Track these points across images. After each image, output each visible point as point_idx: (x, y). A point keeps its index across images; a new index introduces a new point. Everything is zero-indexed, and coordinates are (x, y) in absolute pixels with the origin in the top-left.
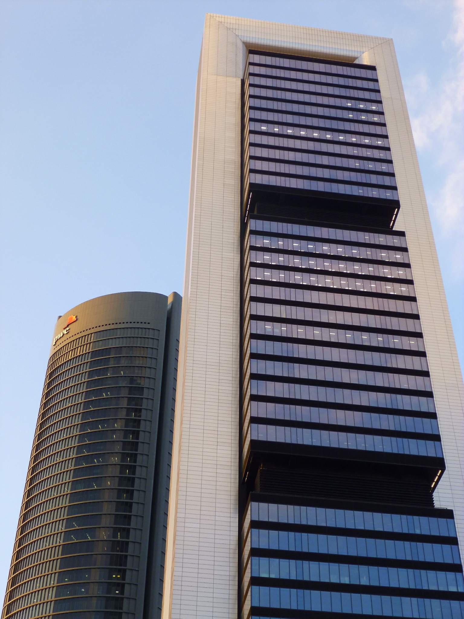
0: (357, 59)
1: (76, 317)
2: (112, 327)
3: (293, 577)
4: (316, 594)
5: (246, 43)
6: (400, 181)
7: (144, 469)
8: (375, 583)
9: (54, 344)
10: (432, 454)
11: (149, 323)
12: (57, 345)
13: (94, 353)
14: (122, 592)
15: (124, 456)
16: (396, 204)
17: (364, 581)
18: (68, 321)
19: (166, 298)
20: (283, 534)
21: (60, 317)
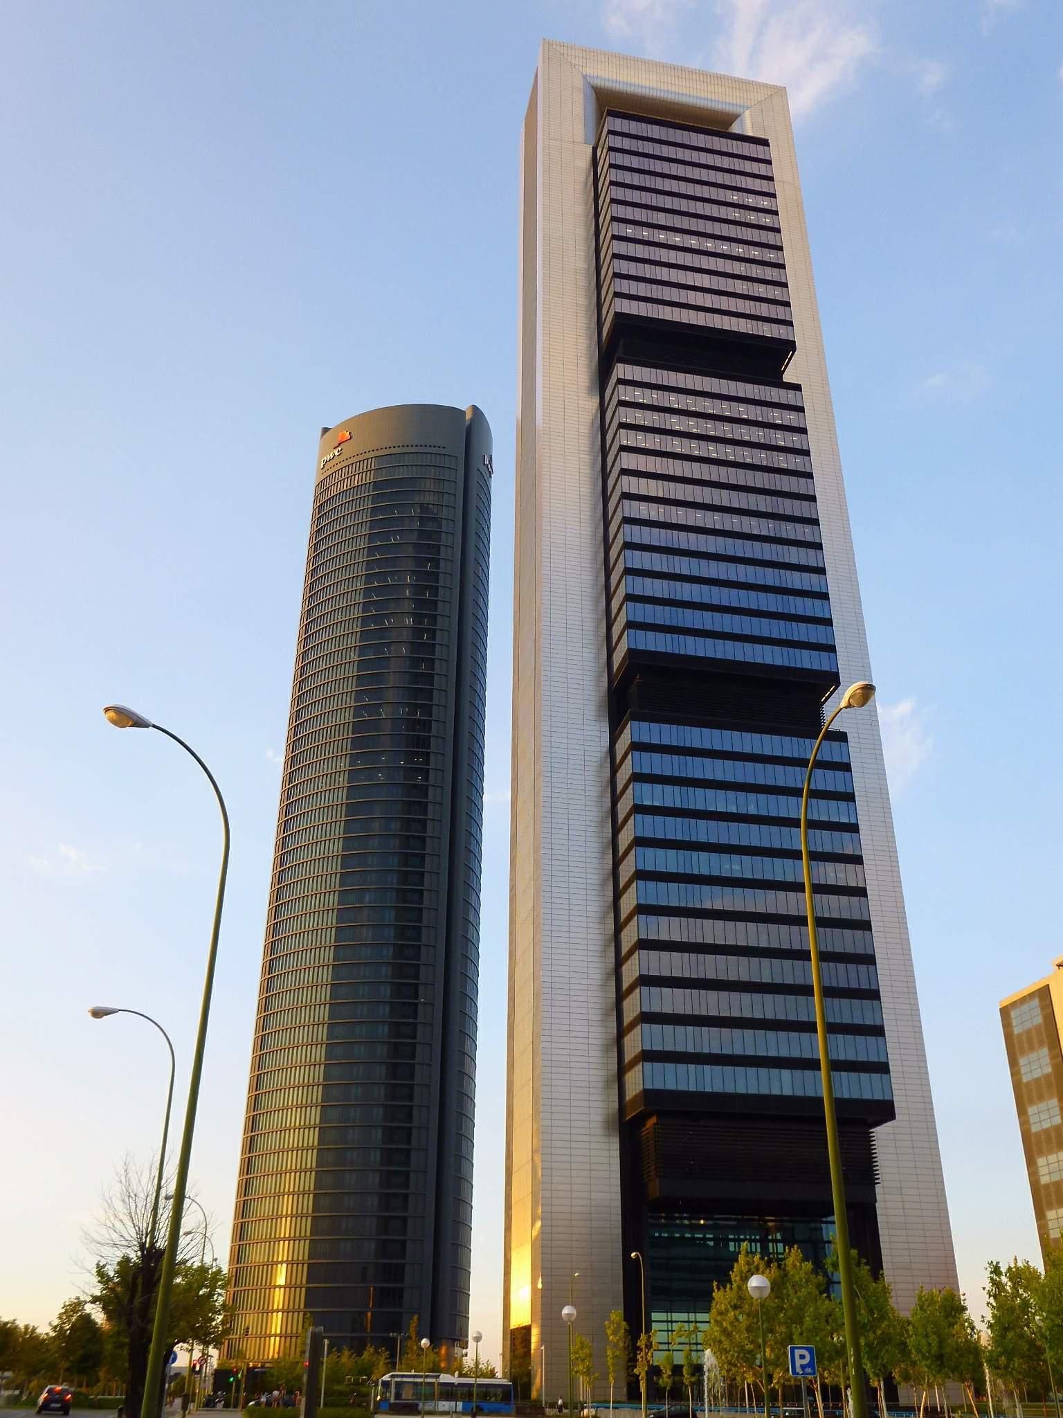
0: (738, 120)
1: (350, 434)
2: (397, 450)
3: (678, 805)
4: (702, 823)
5: (597, 88)
6: (797, 313)
7: (445, 633)
8: (763, 812)
9: (322, 467)
10: (826, 668)
11: (444, 448)
12: (325, 469)
13: (377, 485)
14: (426, 778)
15: (418, 618)
16: (790, 346)
17: (752, 810)
18: (340, 439)
19: (464, 413)
20: (698, 775)
21: (325, 430)
